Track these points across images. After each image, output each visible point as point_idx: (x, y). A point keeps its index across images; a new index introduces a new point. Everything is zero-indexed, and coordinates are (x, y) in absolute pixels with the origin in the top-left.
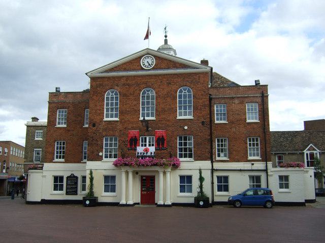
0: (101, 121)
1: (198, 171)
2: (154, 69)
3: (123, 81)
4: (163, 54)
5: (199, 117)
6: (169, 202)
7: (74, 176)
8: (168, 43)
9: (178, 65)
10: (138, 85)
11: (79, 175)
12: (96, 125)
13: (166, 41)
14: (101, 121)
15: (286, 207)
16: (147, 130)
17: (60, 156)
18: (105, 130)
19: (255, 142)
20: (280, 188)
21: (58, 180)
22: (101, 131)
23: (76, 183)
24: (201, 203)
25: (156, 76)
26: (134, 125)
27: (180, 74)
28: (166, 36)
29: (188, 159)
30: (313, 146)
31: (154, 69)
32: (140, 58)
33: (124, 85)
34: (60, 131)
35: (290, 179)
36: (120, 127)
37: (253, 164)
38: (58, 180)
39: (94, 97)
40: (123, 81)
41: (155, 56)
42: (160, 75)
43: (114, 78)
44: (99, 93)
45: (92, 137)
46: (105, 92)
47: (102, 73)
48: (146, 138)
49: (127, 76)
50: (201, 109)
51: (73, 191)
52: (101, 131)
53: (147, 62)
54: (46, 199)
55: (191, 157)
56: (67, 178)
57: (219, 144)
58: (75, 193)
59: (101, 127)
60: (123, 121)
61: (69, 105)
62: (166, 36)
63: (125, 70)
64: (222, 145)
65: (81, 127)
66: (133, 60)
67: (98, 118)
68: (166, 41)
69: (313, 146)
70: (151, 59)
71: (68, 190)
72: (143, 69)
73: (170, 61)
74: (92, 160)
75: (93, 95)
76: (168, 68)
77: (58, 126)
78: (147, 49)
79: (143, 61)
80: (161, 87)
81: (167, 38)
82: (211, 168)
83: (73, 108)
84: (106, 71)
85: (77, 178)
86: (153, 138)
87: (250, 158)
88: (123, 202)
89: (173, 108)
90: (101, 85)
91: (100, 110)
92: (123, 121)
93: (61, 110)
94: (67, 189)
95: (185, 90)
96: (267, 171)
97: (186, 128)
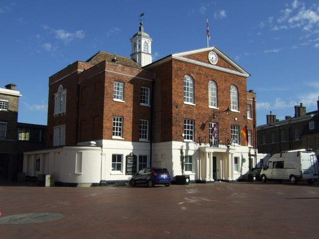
1: (179, 151)
2: (216, 65)
12: (179, 106)
15: (82, 159)
17: (117, 133)
19: (118, 132)
21: (117, 158)
31: (216, 65)
34: (118, 106)
38: (117, 158)
44: (180, 76)
45: (176, 118)
56: (127, 157)
63: (198, 60)
67: (180, 100)
72: (210, 63)
74: (163, 142)
88: (230, 179)
92: (198, 106)
97: (236, 119)
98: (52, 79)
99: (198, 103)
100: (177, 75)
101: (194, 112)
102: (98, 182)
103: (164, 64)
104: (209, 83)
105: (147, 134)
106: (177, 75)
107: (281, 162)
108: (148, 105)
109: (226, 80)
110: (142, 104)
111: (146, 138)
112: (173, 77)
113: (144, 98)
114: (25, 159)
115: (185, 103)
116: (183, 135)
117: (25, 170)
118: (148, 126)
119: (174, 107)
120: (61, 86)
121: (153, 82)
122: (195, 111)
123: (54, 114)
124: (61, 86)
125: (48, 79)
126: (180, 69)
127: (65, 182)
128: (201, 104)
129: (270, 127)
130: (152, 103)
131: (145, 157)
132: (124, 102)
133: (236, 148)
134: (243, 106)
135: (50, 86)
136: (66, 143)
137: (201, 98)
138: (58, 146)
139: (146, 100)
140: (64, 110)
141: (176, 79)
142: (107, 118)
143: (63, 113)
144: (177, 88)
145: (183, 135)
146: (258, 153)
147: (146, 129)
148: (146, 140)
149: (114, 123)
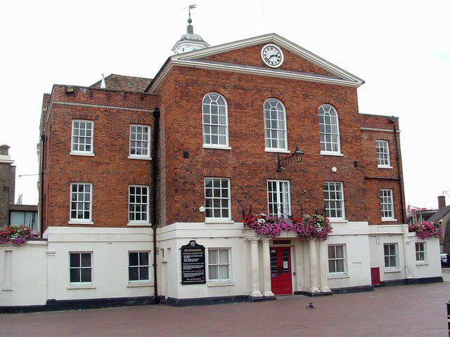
0: (198, 149)
2: (280, 68)
3: (234, 80)
4: (219, 48)
6: (326, 289)
7: (197, 246)
10: (259, 91)
13: (190, 29)
14: (198, 149)
16: (279, 171)
17: (386, 213)
18: (207, 165)
20: (418, 259)
25: (285, 80)
26: (258, 160)
28: (190, 21)
29: (221, 219)
32: (260, 46)
33: (235, 87)
34: (81, 164)
35: (95, 261)
36: (232, 161)
39: (184, 103)
40: (234, 80)
41: (281, 48)
43: (218, 73)
45: (184, 178)
46: (202, 96)
47: (194, 60)
48: (275, 183)
50: (351, 142)
51: (195, 277)
54: (57, 299)
57: (338, 198)
60: (238, 150)
61: (98, 113)
62: (190, 21)
63: (235, 62)
64: (138, 209)
65: (125, 158)
66: (248, 48)
67: (193, 141)
68: (190, 29)
70: (277, 52)
71: (186, 275)
72: (264, 66)
75: (181, 98)
76: (303, 71)
77: (73, 152)
78: (273, 34)
81: (191, 24)
83: (105, 121)
85: (203, 248)
88: (315, 289)
90: (194, 82)
91: (195, 127)
92: (238, 150)
93: (80, 121)
95: (327, 110)
97: (334, 169)
102: (43, 303)
107: (130, 256)
115: (205, 145)
122: (232, 161)
127: (180, 297)
128: (246, 146)
131: (144, 256)
132: (392, 167)
134: (351, 142)
144: (187, 118)
145: (202, 209)
148: (147, 222)
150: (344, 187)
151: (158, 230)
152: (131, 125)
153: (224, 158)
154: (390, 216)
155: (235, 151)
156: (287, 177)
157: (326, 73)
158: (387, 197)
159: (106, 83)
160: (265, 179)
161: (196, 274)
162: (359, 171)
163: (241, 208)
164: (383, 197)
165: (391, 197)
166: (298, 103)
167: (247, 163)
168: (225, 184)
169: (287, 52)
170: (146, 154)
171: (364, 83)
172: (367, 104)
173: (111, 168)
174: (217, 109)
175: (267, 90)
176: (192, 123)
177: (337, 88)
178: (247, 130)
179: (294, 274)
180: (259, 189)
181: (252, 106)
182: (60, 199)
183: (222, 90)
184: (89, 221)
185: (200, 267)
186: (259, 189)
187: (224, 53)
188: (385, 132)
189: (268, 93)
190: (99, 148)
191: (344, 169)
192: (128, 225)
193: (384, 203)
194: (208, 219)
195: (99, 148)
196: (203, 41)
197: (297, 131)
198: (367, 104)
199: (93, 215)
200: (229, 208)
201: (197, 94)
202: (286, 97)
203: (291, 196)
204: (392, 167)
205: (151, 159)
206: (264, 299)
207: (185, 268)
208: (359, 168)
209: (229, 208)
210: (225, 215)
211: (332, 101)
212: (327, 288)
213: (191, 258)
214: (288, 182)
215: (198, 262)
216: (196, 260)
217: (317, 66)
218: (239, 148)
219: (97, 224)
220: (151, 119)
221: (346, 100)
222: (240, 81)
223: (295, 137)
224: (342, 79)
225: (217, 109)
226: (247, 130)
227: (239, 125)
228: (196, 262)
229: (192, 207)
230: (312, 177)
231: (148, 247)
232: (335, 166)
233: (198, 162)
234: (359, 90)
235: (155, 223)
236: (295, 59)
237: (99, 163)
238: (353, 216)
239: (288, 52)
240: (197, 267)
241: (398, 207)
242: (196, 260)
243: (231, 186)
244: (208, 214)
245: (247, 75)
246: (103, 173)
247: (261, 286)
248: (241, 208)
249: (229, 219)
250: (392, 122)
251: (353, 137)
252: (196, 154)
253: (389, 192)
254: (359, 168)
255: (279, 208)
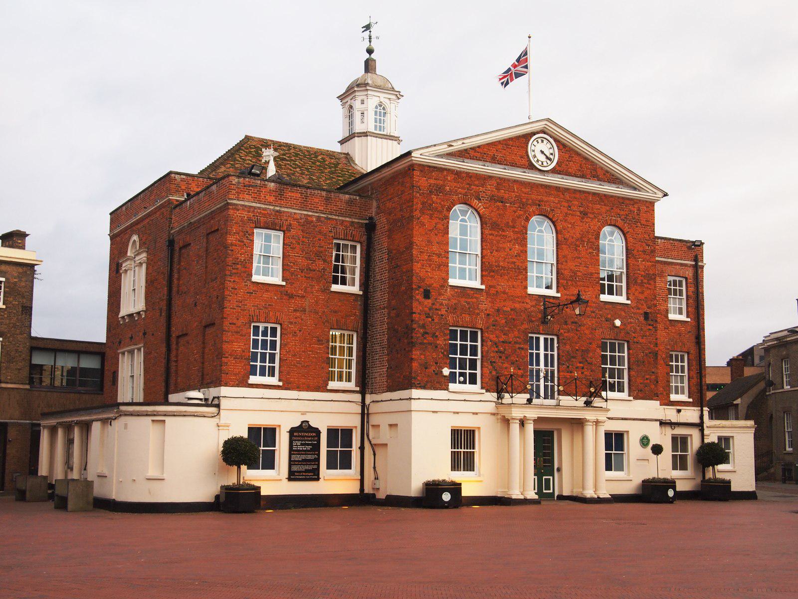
2: (554, 171)
3: (490, 187)
5: (639, 300)
6: (604, 493)
8: (380, 69)
9: (600, 173)
10: (523, 206)
11: (322, 423)
12: (433, 294)
13: (369, 66)
16: (544, 321)
17: (677, 387)
22: (443, 312)
23: (316, 448)
24: (446, 497)
25: (558, 189)
26: (517, 306)
27: (605, 195)
28: (370, 51)
29: (468, 387)
30: (251, 348)
31: (554, 171)
32: (527, 137)
33: (492, 199)
36: (485, 305)
37: (679, 411)
41: (556, 140)
42: (567, 190)
45: (423, 326)
48: (538, 339)
49: (623, 198)
51: (306, 471)
52: (443, 312)
53: (541, 151)
55: (273, 375)
56: (292, 432)
58: (315, 475)
59: (443, 300)
60: (493, 291)
62: (370, 51)
63: (494, 160)
68: (369, 66)
69: (251, 348)
70: (549, 146)
71: (295, 468)
72: (532, 167)
73: (586, 159)
78: (549, 120)
79: (533, 148)
80: (569, 218)
81: (373, 56)
82: (412, 410)
83: (300, 233)
84: (463, 154)
85: (317, 432)
86: (552, 340)
87: (674, 397)
88: (589, 493)
89: (591, 274)
90: (440, 189)
91: (439, 255)
94: (291, 463)
96: (703, 427)
97: (618, 323)
98: (116, 216)
99: (494, 283)
100: (427, 207)
101: (483, 307)
103: (394, 177)
104: (530, 226)
105: (353, 371)
106: (427, 207)
108: (355, 289)
109: (585, 214)
110: (335, 288)
111: (349, 380)
112: (417, 213)
113: (343, 272)
114: (45, 436)
116: (446, 371)
117: (43, 470)
118: (355, 346)
119: (419, 296)
120: (135, 238)
121: (370, 227)
122: (485, 305)
123: (122, 314)
124: (135, 238)
125: (108, 218)
126: (440, 189)
128: (503, 284)
129: (781, 343)
130: (365, 284)
131: (347, 433)
132: (689, 320)
133: (610, 405)
135: (113, 238)
136: (146, 390)
137: (504, 268)
138: (699, 354)
139: (348, 276)
140: (140, 306)
141: (425, 219)
142: (233, 328)
143: (138, 313)
145: (446, 371)
146: (711, 418)
147: (350, 354)
148: (352, 385)
149: (256, 342)
150: (629, 349)
151: (369, 398)
152: (335, 241)
153: (475, 300)
154: (683, 393)
155: (490, 292)
156: (555, 331)
157: (613, 178)
158: (680, 364)
159: (278, 166)
160: (526, 333)
161: (307, 467)
162: (651, 327)
163: (494, 373)
164: (674, 363)
165: (686, 364)
166: (573, 224)
167: (505, 308)
168: (474, 339)
169: (562, 145)
170: (354, 285)
171: (666, 195)
172: (668, 223)
173: (307, 303)
174: (465, 230)
175: (534, 204)
176: (435, 248)
177: (628, 202)
178: (503, 257)
179: (559, 470)
180: (518, 346)
181: (514, 227)
182: (237, 347)
183: (475, 202)
184: (274, 381)
185: (313, 457)
186: (518, 346)
187: (479, 147)
188: (682, 265)
189: (534, 208)
190: (292, 274)
191: (631, 323)
192: (329, 387)
193: (674, 374)
194: (452, 386)
195: (292, 274)
196: (393, 89)
197: (571, 265)
198: (668, 223)
199: (280, 372)
200: (478, 372)
201: (443, 206)
202: (558, 215)
203: (558, 359)
204: (689, 320)
205: (361, 293)
206: (525, 502)
207: (294, 457)
208: (651, 323)
209: (478, 372)
210: (473, 381)
211: (620, 223)
212: (605, 492)
213: (302, 444)
214: (555, 338)
215: (311, 450)
216: (309, 448)
217: (602, 168)
218: (493, 287)
219: (287, 385)
220: (361, 234)
221: (638, 221)
222: (498, 189)
223: (567, 273)
224: (635, 189)
225: (465, 230)
226: (503, 257)
227: (495, 253)
228: (308, 451)
229: (433, 368)
230: (587, 332)
231: (353, 421)
232: (619, 318)
233: (442, 304)
234: (656, 204)
235: (364, 386)
236: (574, 158)
237: (291, 296)
238: (639, 392)
239: (564, 146)
240: (309, 457)
241: (695, 381)
242: (309, 448)
243: (482, 341)
244: (452, 378)
245: (509, 180)
246: (295, 310)
247: (523, 486)
248: (494, 373)
249: (477, 388)
250: (694, 249)
251: (645, 277)
252: (440, 294)
253: (682, 357)
254: (651, 323)
255: (542, 375)
